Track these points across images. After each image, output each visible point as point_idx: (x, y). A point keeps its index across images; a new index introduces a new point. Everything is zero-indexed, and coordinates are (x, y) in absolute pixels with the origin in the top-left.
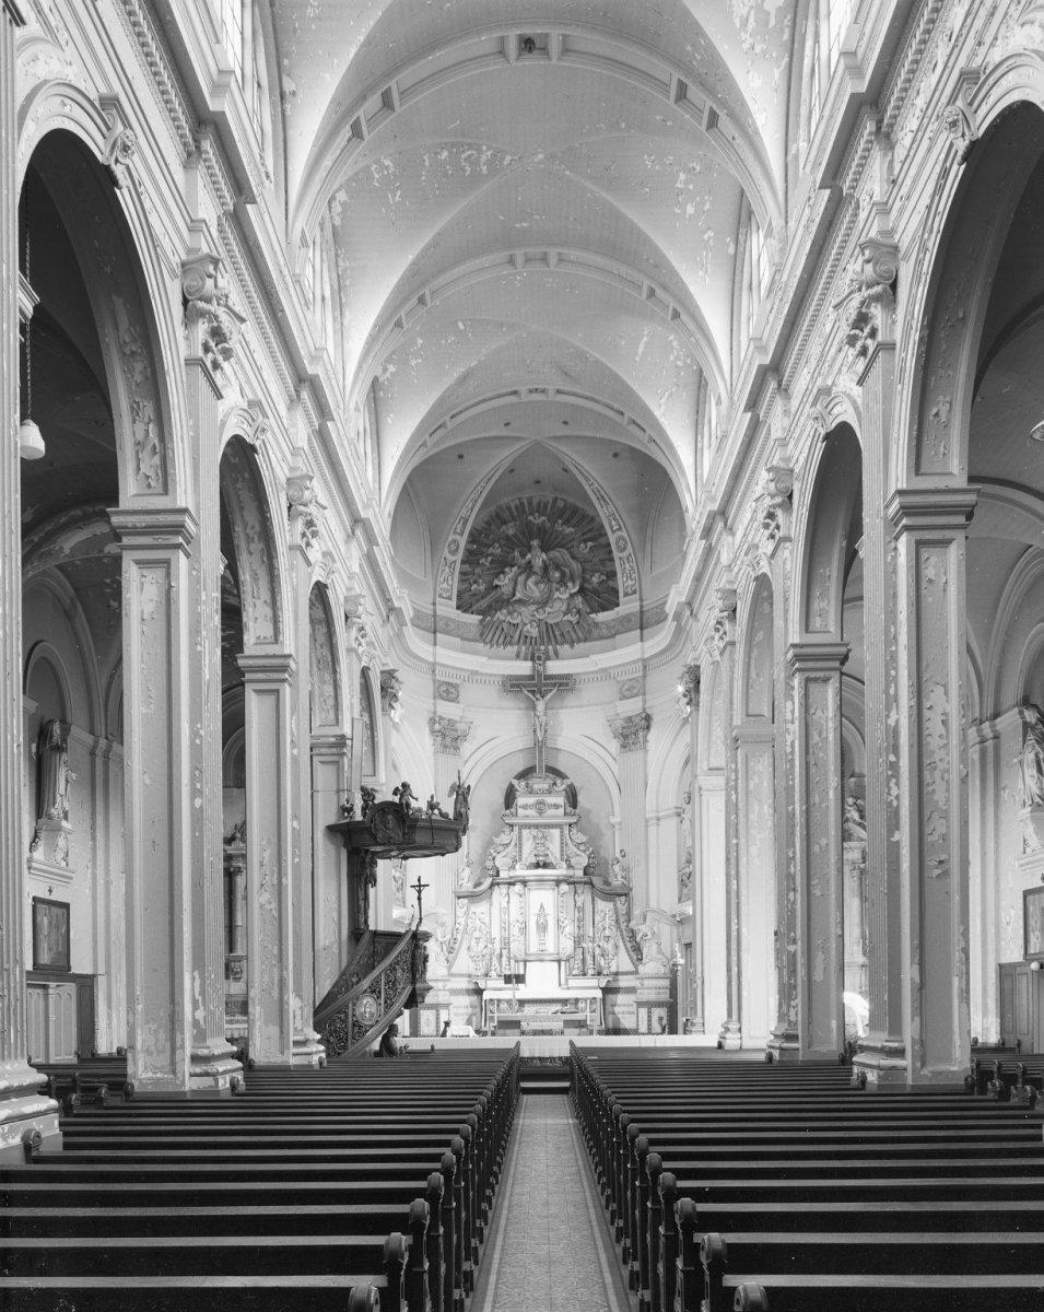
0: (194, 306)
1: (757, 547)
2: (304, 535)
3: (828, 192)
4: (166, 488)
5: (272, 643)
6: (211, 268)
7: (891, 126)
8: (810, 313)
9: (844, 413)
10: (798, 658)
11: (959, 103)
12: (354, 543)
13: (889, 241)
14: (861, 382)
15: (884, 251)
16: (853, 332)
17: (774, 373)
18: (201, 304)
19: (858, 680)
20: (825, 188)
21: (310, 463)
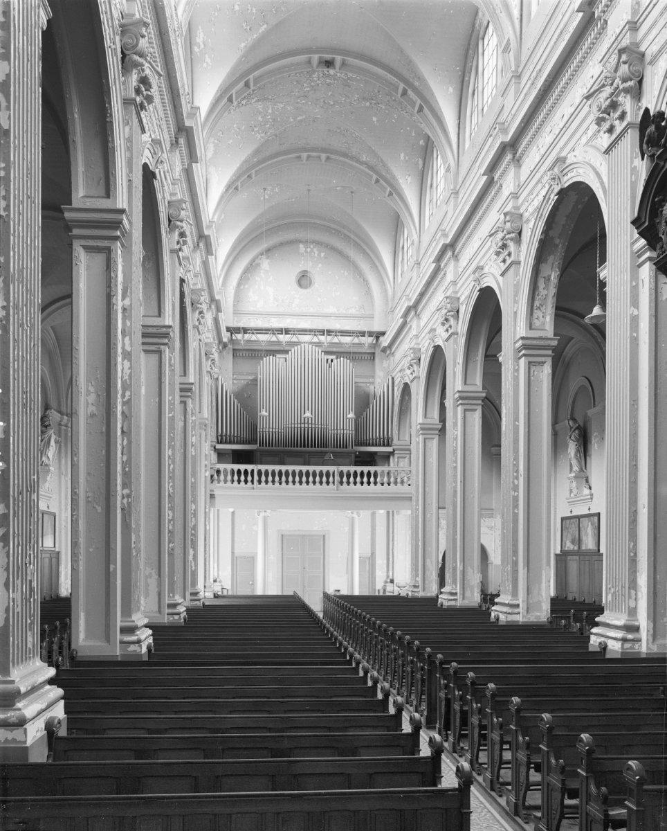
0: (130, 59)
1: (435, 330)
2: (178, 243)
3: (486, 177)
4: (108, 191)
5: (156, 316)
6: (144, 29)
7: (521, 157)
8: (481, 213)
9: (489, 282)
10: (422, 429)
11: (556, 170)
12: (198, 253)
13: (517, 212)
14: (503, 274)
15: (515, 217)
16: (601, 115)
17: (451, 248)
18: (136, 58)
19: (594, 404)
20: (581, 11)
21: (180, 193)
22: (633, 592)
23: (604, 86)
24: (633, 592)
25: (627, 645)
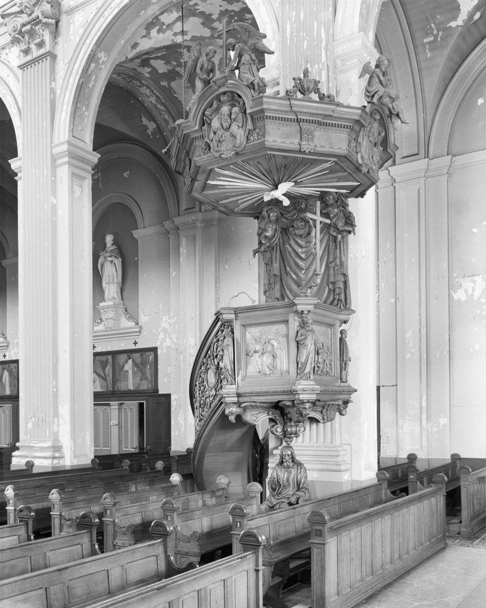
22: (56, 420)
23: (21, 12)
24: (56, 420)
25: (56, 461)
